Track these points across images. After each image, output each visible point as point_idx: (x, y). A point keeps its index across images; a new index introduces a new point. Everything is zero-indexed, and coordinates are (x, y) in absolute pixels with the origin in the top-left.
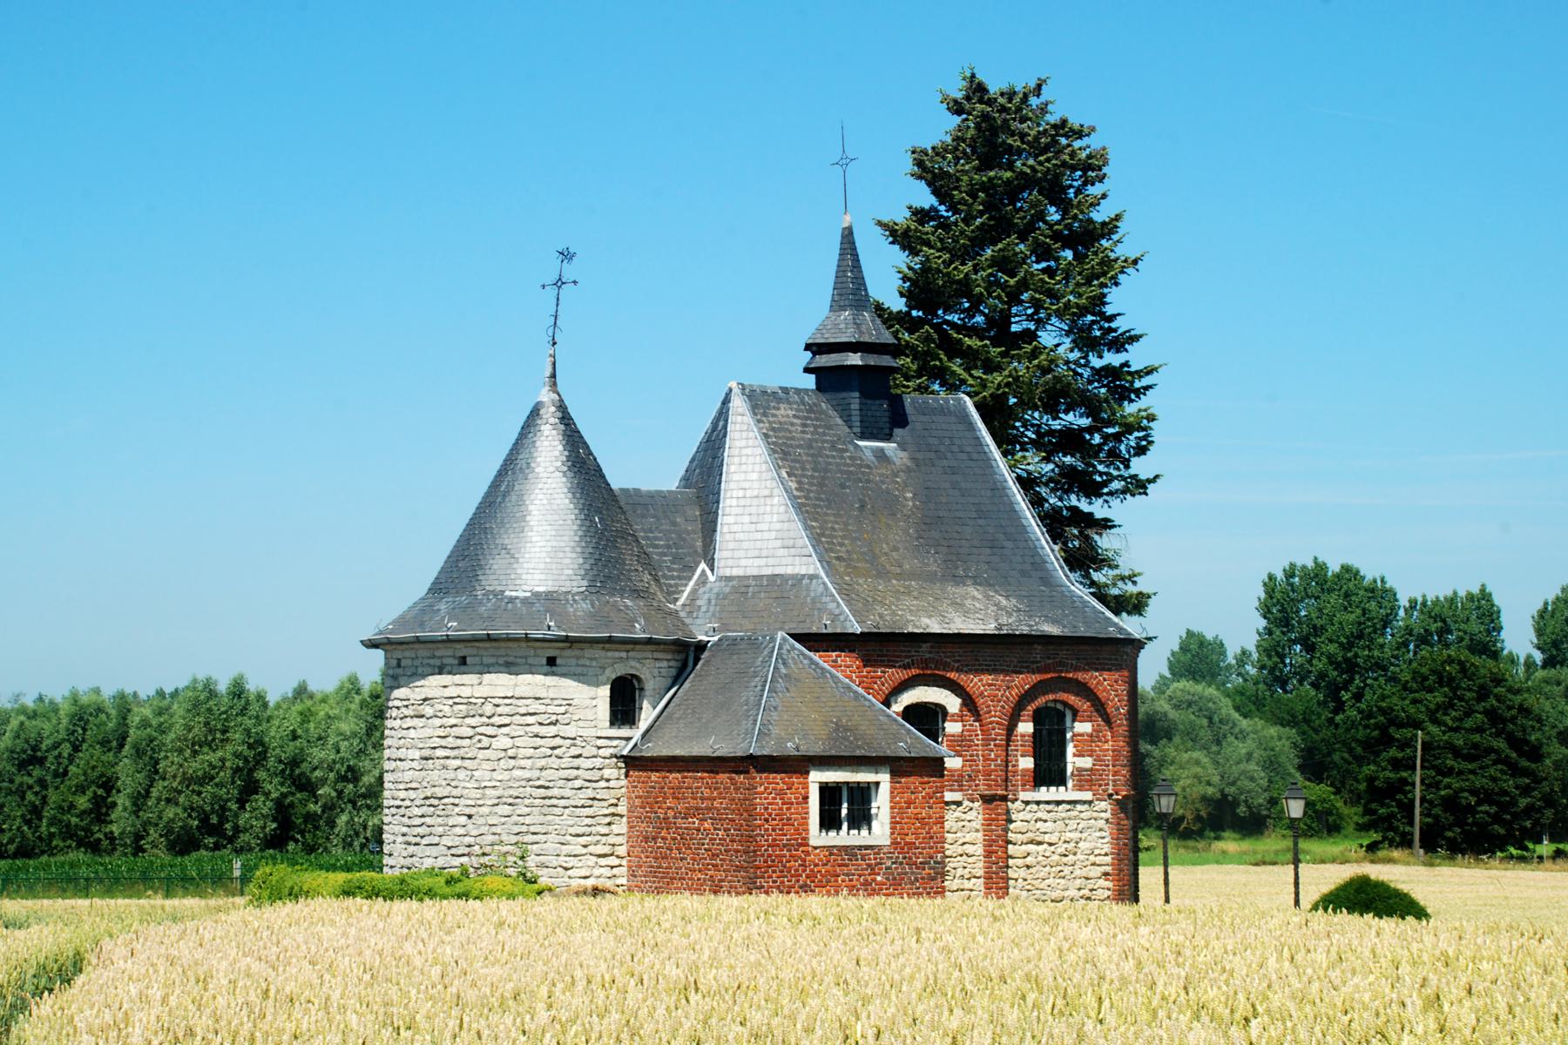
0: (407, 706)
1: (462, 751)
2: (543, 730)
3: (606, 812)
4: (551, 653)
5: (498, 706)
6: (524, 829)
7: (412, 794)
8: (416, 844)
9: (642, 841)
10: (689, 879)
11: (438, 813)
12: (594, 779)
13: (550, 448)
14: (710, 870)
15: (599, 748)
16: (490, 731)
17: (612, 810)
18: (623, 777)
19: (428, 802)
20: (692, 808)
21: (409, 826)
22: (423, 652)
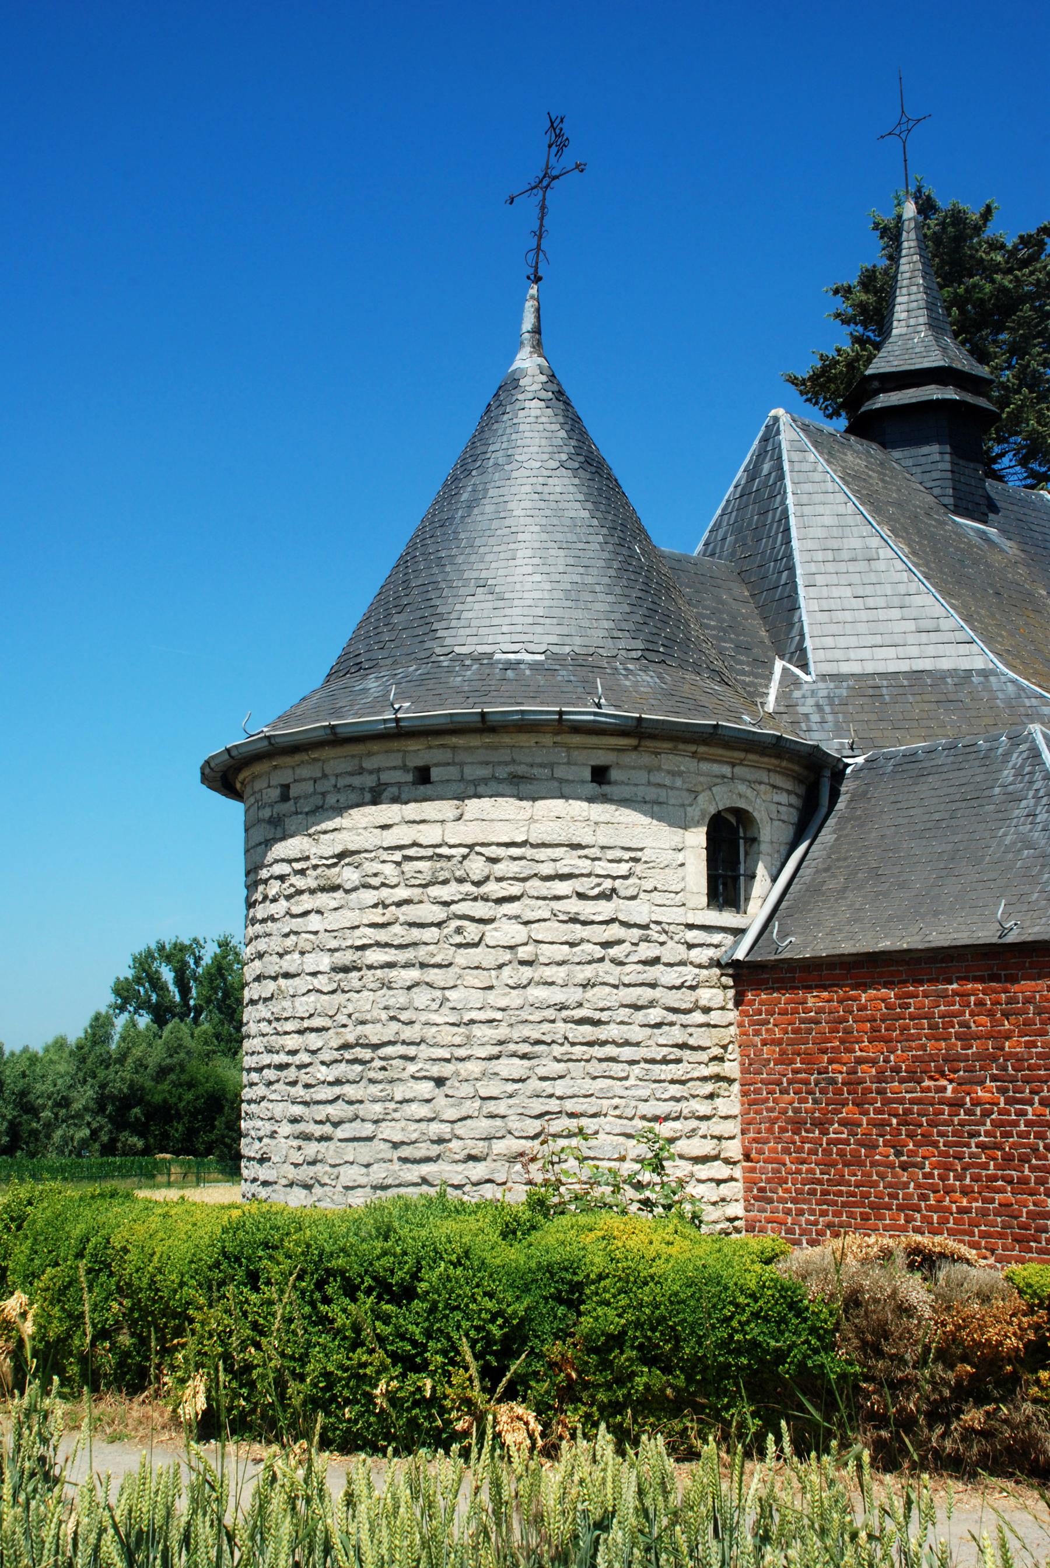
0: (302, 872)
2: (587, 909)
3: (706, 1072)
4: (601, 758)
5: (494, 861)
6: (554, 1105)
7: (314, 1040)
8: (324, 1138)
9: (783, 1130)
10: (929, 1208)
11: (372, 1074)
12: (684, 1006)
15: (690, 946)
16: (480, 910)
17: (713, 1069)
18: (730, 1005)
19: (348, 1056)
20: (932, 1058)
21: (306, 1104)
22: (337, 761)
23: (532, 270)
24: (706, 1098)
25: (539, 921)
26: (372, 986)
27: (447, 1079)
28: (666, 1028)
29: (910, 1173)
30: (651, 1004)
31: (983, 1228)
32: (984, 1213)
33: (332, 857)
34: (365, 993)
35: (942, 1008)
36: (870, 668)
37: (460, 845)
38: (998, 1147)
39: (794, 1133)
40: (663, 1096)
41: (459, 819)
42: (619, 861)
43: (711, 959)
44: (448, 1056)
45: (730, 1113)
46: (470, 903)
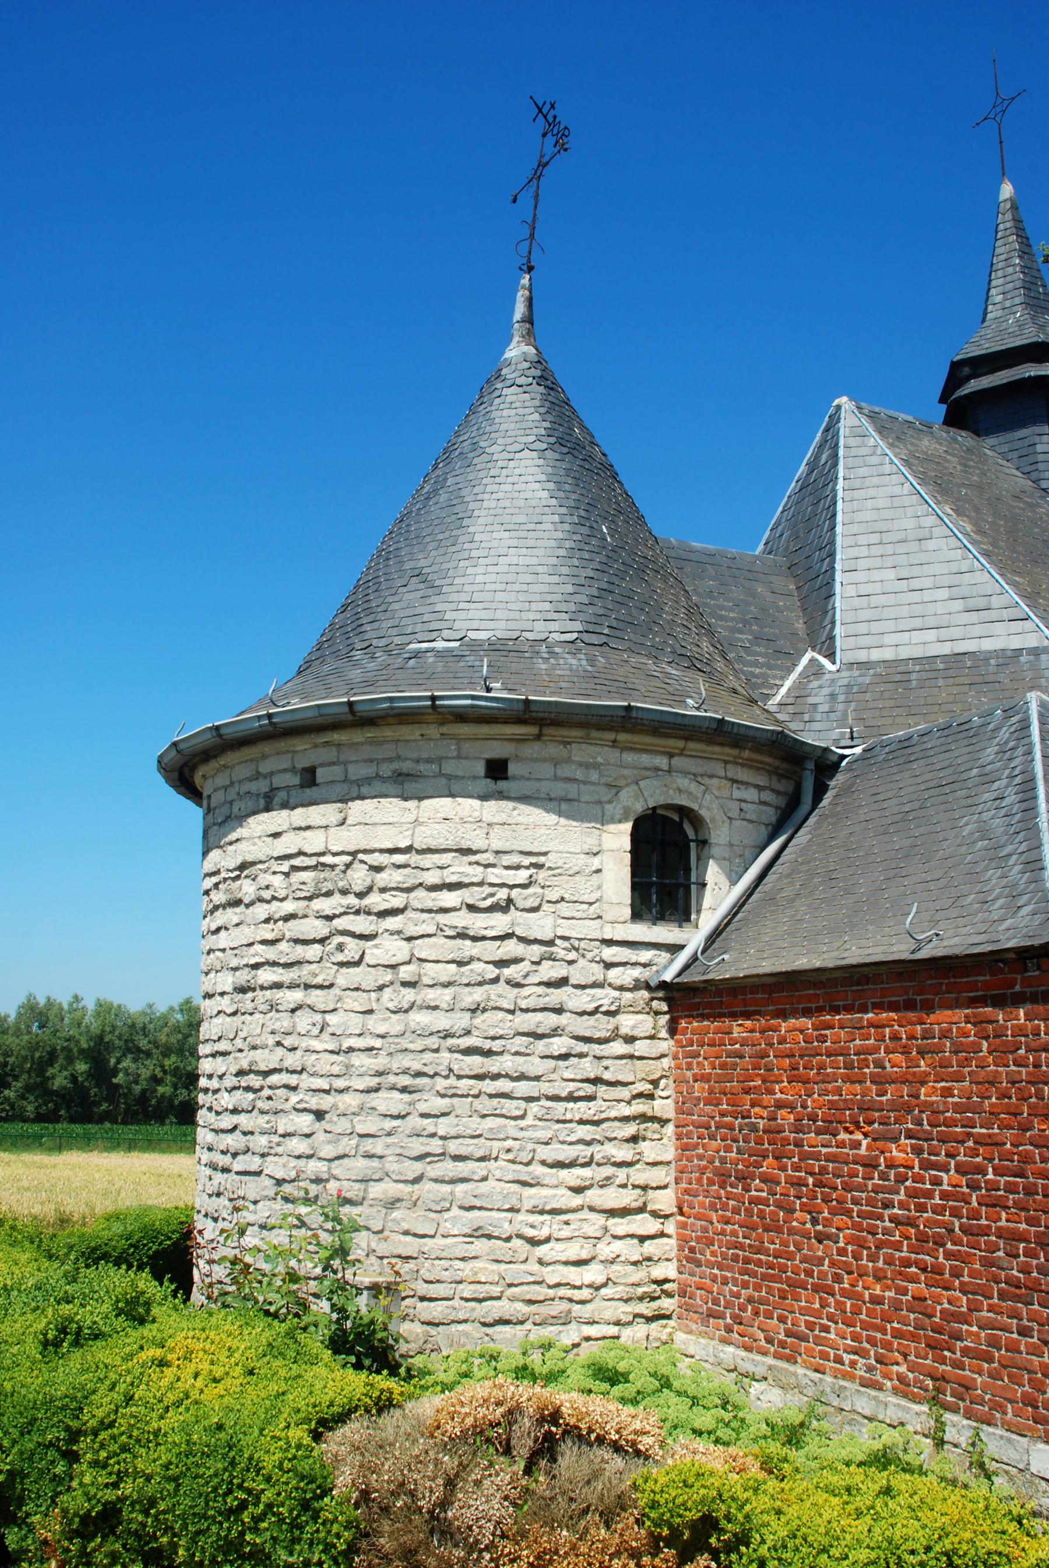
1: (307, 969)
2: (478, 923)
3: (627, 1111)
4: (497, 750)
5: (378, 869)
6: (435, 1146)
9: (711, 1182)
10: (844, 1293)
11: (260, 1104)
12: (597, 1035)
13: (517, 418)
14: (914, 1280)
15: (609, 966)
16: (361, 924)
17: (639, 1107)
18: (663, 1034)
20: (848, 1105)
23: (525, 261)
24: (627, 1141)
25: (422, 936)
26: (262, 1008)
27: (326, 1112)
28: (573, 1060)
29: (826, 1246)
30: (555, 1032)
31: (895, 1325)
32: (897, 1306)
33: (235, 869)
34: (257, 1016)
35: (858, 1042)
36: (904, 653)
37: (342, 853)
38: (911, 1223)
39: (721, 1187)
40: (569, 1139)
41: (343, 824)
42: (518, 867)
43: (637, 980)
44: (327, 1087)
45: (659, 1159)
46: (352, 917)
